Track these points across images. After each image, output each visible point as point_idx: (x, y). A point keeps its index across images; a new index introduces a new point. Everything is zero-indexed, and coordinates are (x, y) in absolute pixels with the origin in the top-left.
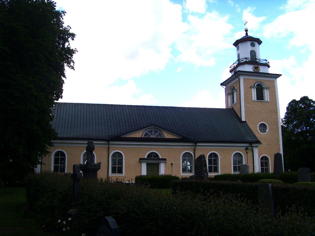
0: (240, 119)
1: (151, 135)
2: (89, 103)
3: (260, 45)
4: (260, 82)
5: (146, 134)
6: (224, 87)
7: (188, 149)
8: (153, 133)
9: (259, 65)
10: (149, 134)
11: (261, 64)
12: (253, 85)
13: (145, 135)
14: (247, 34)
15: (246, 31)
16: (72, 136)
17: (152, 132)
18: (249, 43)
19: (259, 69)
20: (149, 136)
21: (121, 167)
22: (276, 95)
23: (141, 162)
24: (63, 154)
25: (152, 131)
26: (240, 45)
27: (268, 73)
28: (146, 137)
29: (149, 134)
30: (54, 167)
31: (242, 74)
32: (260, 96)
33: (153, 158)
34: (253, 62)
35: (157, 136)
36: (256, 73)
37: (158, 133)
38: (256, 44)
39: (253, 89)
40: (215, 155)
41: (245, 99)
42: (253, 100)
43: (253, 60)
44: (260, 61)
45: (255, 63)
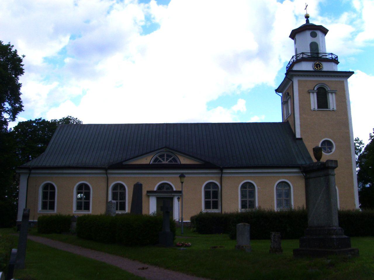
0: (294, 135)
1: (162, 160)
2: (203, 122)
3: (325, 35)
4: (322, 83)
5: (156, 160)
6: (281, 94)
7: (212, 178)
8: (165, 157)
9: (323, 61)
10: (160, 159)
11: (325, 60)
12: (313, 89)
13: (155, 161)
14: (307, 21)
15: (307, 17)
16: (63, 164)
17: (164, 157)
18: (308, 33)
19: (322, 67)
20: (160, 161)
21: (254, 200)
22: (346, 100)
23: (148, 196)
24: (53, 187)
25: (164, 155)
26: (297, 37)
27: (336, 70)
28: (156, 163)
29: (160, 159)
30: (205, 202)
31: (296, 76)
32: (323, 103)
33: (165, 190)
34: (314, 57)
35: (170, 161)
36: (318, 72)
37: (172, 158)
38: (319, 34)
39: (311, 94)
40: (251, 185)
41: (301, 107)
42: (312, 109)
43: (316, 56)
44: (323, 56)
45: (316, 59)
